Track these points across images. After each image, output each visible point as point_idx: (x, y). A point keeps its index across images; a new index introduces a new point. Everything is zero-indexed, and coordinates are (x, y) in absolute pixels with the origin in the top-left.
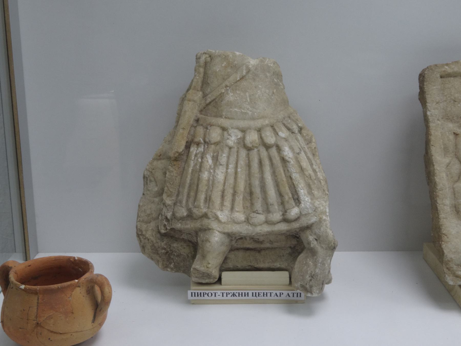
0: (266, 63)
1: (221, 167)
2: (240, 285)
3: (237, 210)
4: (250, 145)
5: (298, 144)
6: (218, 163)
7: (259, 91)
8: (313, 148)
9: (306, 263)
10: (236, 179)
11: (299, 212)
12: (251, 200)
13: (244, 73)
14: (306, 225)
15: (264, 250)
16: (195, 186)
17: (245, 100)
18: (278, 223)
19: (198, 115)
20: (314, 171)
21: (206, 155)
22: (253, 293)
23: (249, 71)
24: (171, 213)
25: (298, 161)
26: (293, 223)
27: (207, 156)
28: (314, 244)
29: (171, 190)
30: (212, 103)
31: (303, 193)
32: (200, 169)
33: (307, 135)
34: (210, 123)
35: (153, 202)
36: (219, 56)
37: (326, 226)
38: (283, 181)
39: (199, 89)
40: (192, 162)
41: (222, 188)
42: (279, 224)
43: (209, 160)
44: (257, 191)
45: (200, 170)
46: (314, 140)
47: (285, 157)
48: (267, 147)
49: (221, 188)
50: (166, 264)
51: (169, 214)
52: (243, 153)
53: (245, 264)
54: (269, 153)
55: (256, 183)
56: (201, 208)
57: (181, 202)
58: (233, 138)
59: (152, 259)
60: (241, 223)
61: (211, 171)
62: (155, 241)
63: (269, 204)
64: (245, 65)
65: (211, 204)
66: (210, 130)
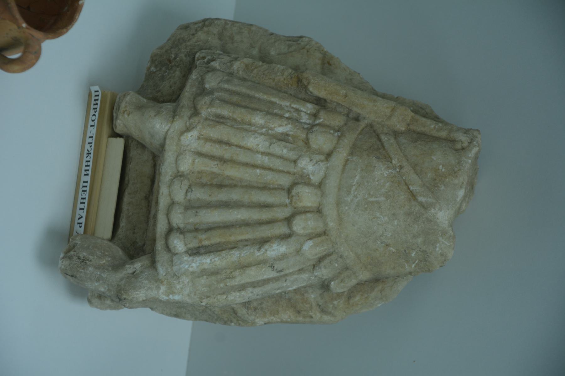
0: (440, 239)
1: (267, 144)
2: (104, 165)
3: (197, 161)
4: (294, 192)
5: (291, 271)
6: (274, 140)
7: (386, 218)
8: (311, 314)
9: (106, 255)
10: (246, 165)
11: (177, 251)
12: (212, 185)
13: (421, 199)
14: (157, 260)
15: (148, 206)
16: (248, 103)
17: (372, 193)
18: (168, 220)
19: (366, 121)
20: (242, 287)
21: (292, 124)
22: (87, 182)
23: (425, 207)
24: (218, 67)
25: (260, 263)
26: (163, 242)
27: (290, 126)
28: (129, 269)
29: (255, 71)
30: (378, 143)
31: (204, 261)
32: (270, 111)
33: (335, 308)
34: (345, 136)
35: (252, 46)
36: (459, 163)
37: (149, 288)
38: (230, 236)
39: (411, 127)
40: (288, 104)
41: (233, 141)
42: (167, 221)
43: (282, 128)
44: (223, 196)
45: (268, 113)
46: (326, 318)
47: (268, 244)
48: (289, 220)
49: (234, 140)
50: (156, 60)
51: (217, 64)
52: (285, 181)
53: (131, 175)
54: (280, 221)
55: (235, 195)
56: (208, 108)
57: (228, 82)
58: (310, 168)
59: (168, 40)
60: (176, 164)
61: (264, 130)
62: (188, 44)
63: (198, 210)
64: (434, 201)
65: (211, 123)
66: (333, 134)
